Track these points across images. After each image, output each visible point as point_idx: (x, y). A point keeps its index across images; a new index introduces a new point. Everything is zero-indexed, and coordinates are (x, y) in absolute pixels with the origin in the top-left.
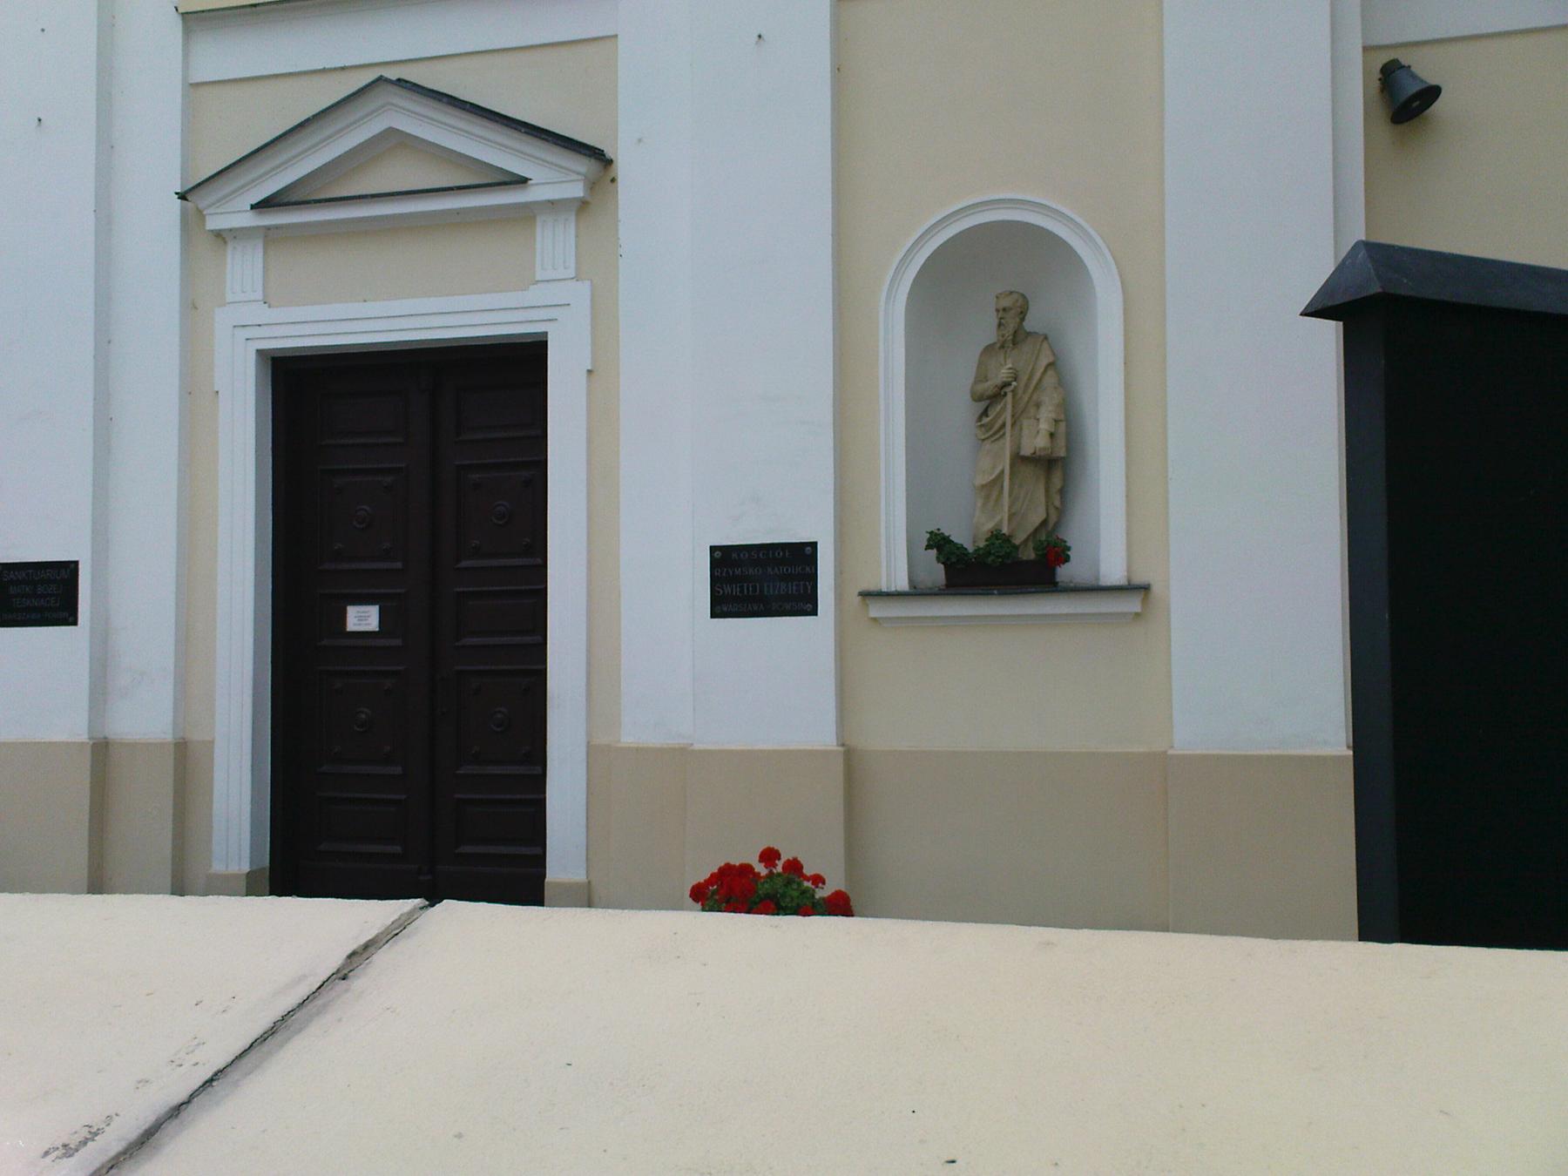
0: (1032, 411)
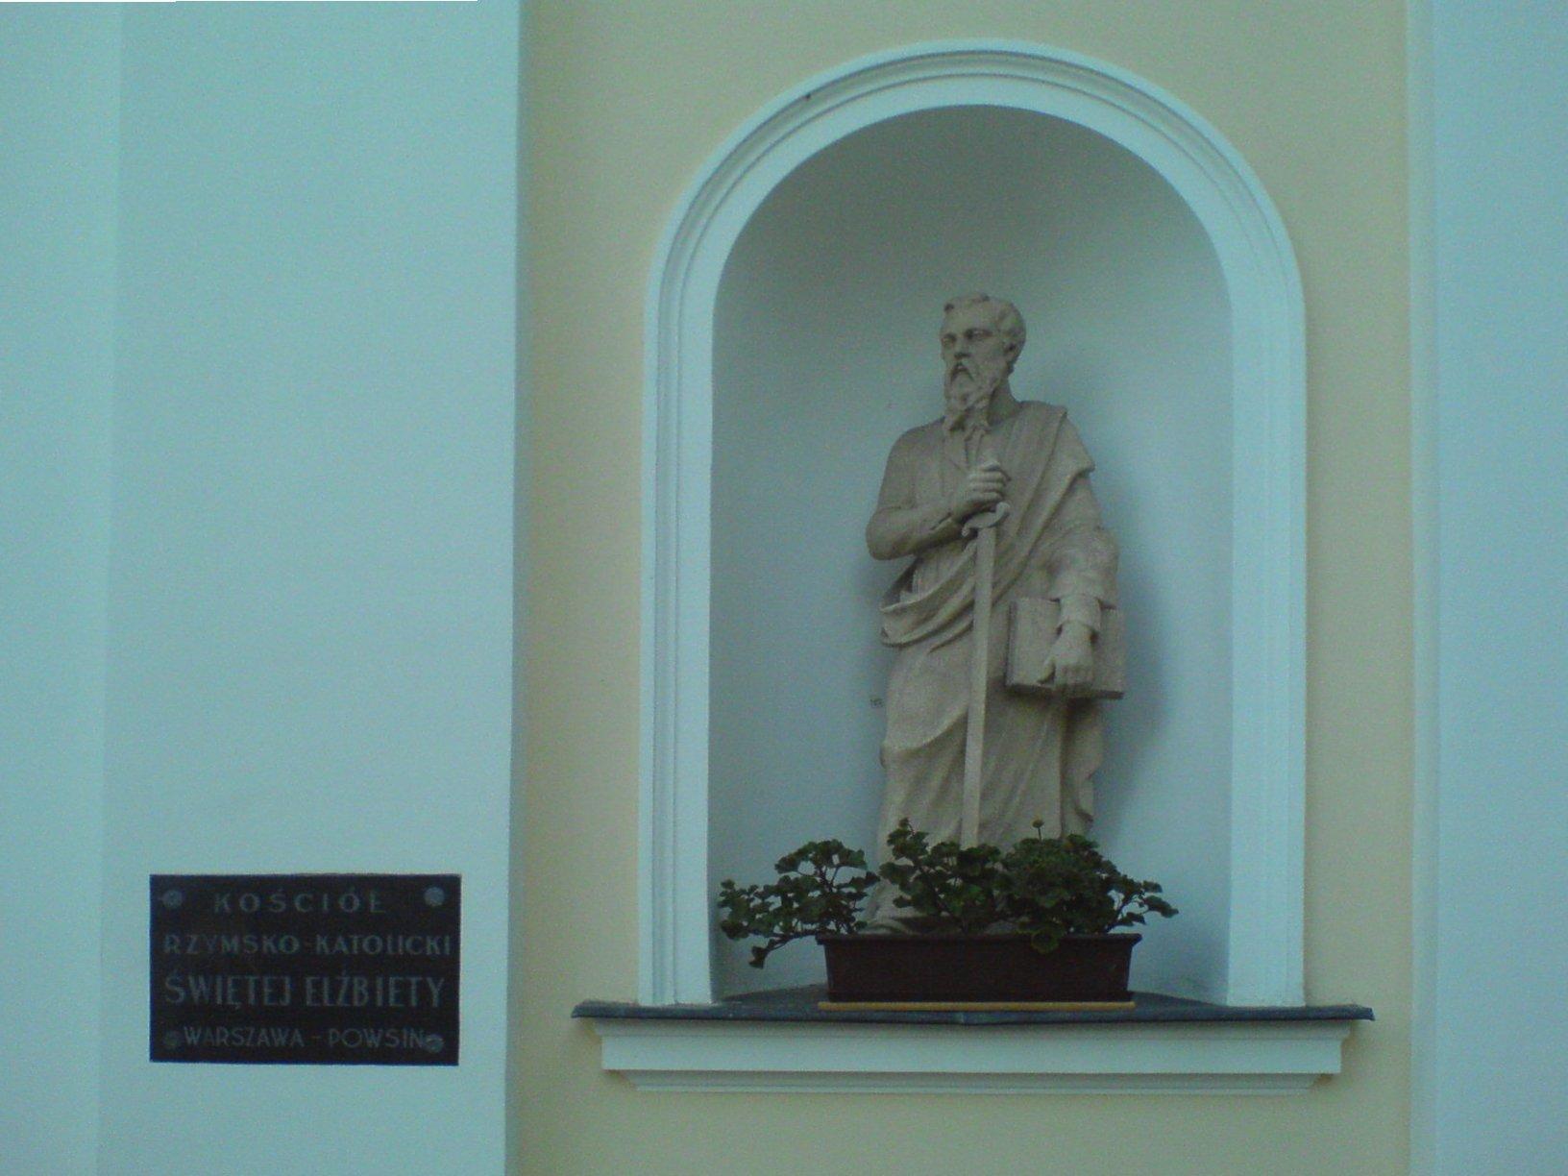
0: (1037, 579)
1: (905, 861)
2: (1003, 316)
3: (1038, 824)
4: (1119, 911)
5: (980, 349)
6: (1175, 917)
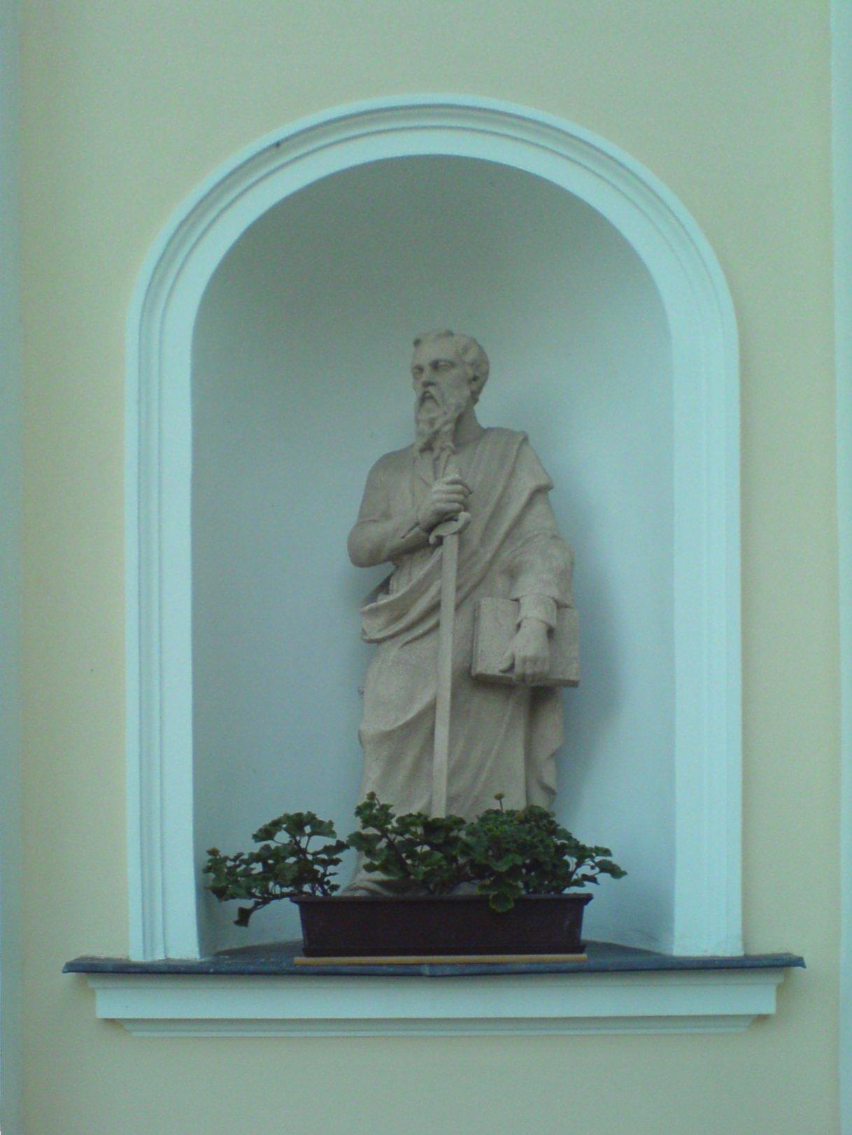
1: (371, 831)
2: (466, 350)
3: (499, 797)
4: (572, 873)
5: (445, 379)
6: (623, 879)
